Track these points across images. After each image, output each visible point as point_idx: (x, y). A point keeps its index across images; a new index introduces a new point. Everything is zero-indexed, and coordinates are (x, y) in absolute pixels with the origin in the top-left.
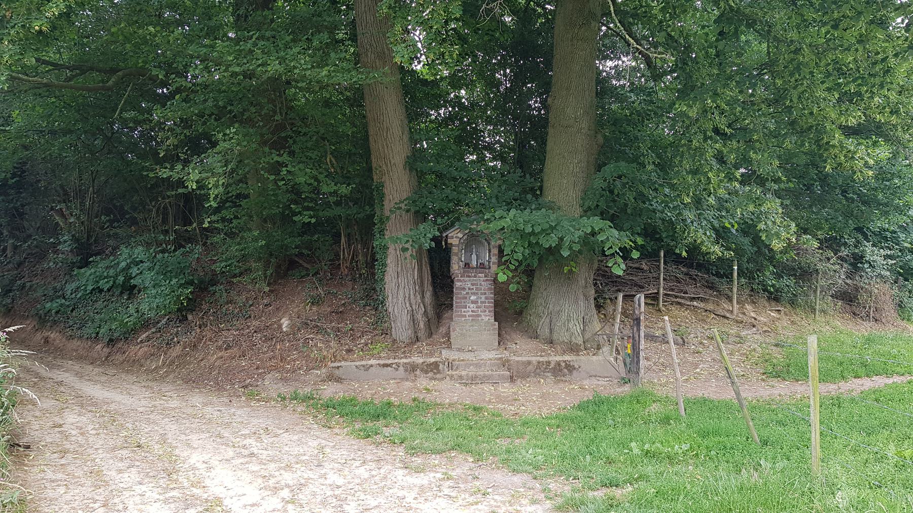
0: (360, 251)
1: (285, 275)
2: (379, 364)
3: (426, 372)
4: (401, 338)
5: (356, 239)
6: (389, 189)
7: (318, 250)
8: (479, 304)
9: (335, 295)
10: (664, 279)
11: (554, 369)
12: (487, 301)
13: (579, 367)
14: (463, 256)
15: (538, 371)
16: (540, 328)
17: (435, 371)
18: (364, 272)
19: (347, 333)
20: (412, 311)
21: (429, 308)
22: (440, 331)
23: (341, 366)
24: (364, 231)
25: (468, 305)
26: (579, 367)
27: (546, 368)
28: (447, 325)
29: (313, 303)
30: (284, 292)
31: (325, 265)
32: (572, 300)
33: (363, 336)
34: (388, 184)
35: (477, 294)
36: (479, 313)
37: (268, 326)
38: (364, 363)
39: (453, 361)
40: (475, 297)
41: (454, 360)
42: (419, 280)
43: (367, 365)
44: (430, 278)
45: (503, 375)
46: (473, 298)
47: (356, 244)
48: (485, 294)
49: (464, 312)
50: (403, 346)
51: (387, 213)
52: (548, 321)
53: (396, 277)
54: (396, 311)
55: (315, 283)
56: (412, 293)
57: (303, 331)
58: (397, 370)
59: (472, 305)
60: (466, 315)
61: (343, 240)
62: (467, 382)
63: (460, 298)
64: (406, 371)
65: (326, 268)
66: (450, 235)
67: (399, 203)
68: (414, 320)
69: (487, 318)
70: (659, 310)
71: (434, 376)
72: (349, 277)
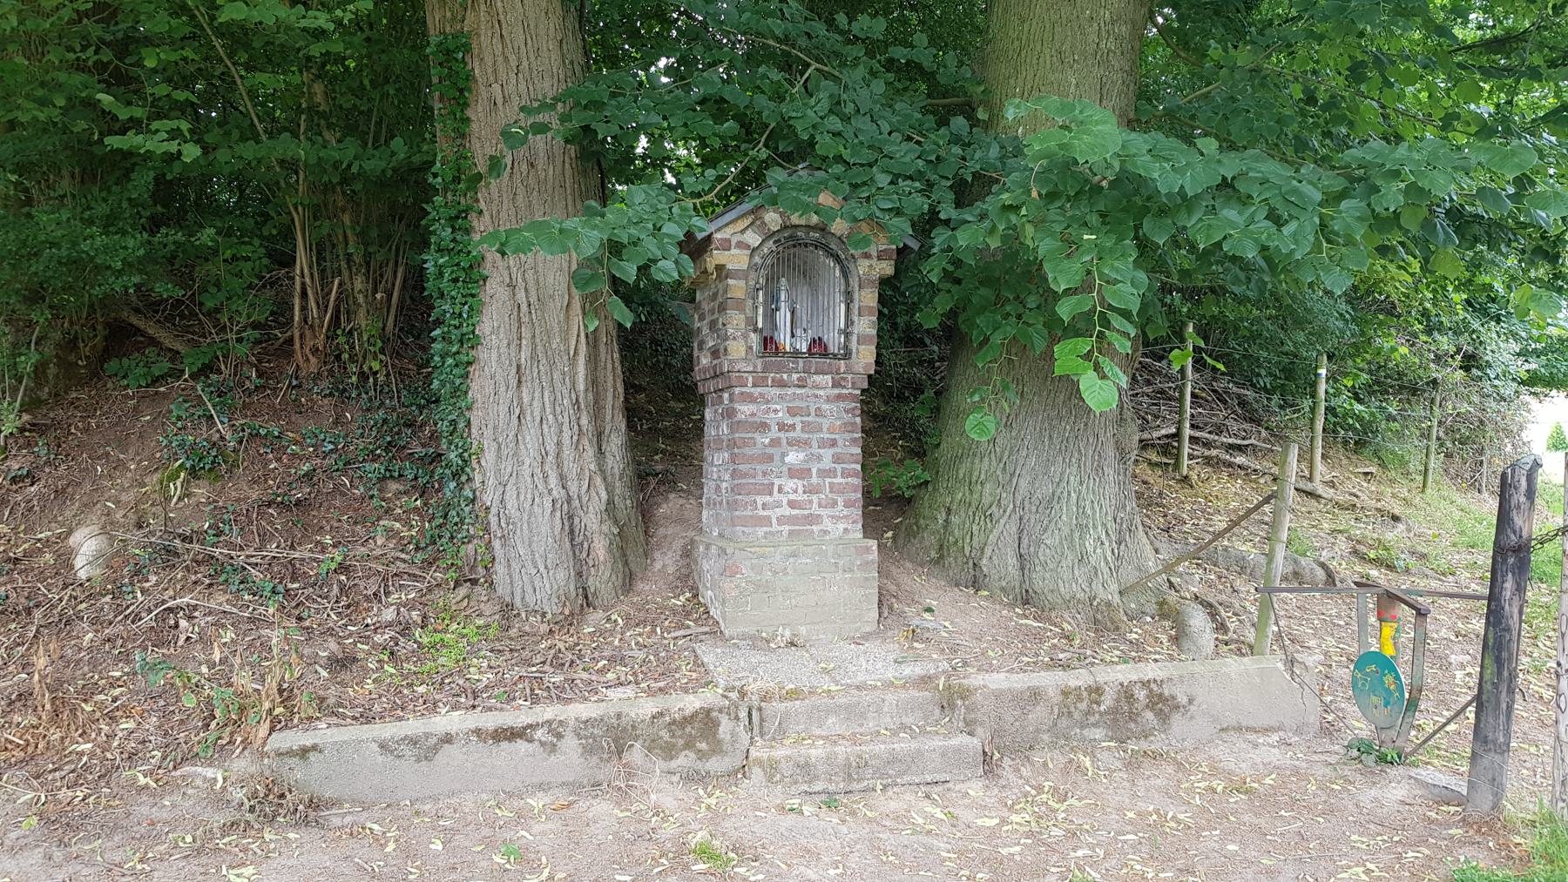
0: (361, 299)
1: (96, 373)
2: (478, 732)
3: (669, 752)
4: (530, 599)
5: (349, 257)
6: (489, 60)
7: (213, 290)
8: (814, 480)
9: (276, 444)
10: (1193, 395)
11: (1114, 711)
12: (839, 467)
13: (1191, 701)
14: (761, 311)
16: (988, 552)
17: (703, 746)
18: (376, 366)
19: (326, 582)
20: (569, 500)
21: (619, 488)
22: (658, 566)
23: (314, 748)
24: (374, 233)
25: (777, 482)
26: (1191, 701)
27: (1088, 713)
28: (678, 545)
29: (193, 473)
30: (86, 430)
31: (240, 340)
32: (1089, 463)
33: (387, 594)
34: (485, 40)
35: (807, 443)
37: (17, 560)
38: (413, 726)
40: (801, 456)
41: (766, 697)
42: (590, 395)
43: (427, 735)
44: (621, 390)
45: (957, 750)
46: (794, 457)
47: (346, 273)
48: (834, 443)
49: (764, 506)
50: (544, 628)
52: (1014, 529)
53: (514, 382)
55: (201, 403)
56: (566, 441)
57: (153, 579)
58: (552, 749)
59: (790, 484)
60: (768, 518)
62: (832, 788)
63: (751, 459)
64: (588, 751)
65: (242, 349)
66: (718, 236)
67: (538, 111)
68: (572, 532)
69: (841, 526)
70: (1185, 479)
72: (325, 384)
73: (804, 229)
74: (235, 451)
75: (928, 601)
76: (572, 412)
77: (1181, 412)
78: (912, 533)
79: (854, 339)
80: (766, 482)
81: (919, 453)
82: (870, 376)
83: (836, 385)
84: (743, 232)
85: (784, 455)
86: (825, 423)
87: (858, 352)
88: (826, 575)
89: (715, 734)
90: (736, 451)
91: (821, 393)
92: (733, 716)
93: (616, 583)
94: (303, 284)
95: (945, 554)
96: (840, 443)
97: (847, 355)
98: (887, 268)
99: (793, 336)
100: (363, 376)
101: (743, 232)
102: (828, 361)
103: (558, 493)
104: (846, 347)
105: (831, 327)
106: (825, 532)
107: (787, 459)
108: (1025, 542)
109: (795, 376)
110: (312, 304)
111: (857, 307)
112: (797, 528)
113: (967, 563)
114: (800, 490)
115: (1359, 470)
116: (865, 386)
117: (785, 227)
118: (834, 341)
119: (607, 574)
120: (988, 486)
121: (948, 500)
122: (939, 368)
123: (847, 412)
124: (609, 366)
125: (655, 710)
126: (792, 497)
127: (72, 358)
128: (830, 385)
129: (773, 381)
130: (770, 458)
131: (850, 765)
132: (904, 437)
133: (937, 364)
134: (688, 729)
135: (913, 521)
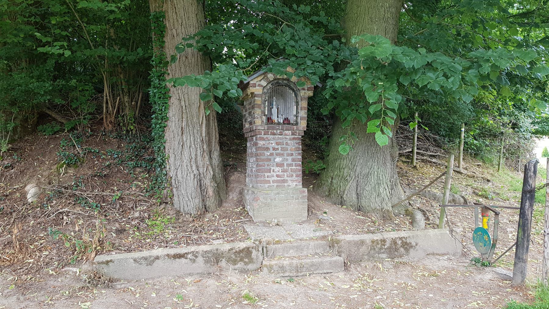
0: (127, 104)
1: (34, 130)
2: (168, 255)
3: (235, 262)
4: (186, 209)
6: (171, 21)
7: (75, 101)
8: (285, 167)
9: (97, 155)
10: (418, 138)
11: (390, 248)
12: (294, 163)
13: (416, 245)
15: (372, 252)
16: (346, 192)
17: (247, 260)
18: (132, 128)
19: (115, 203)
20: (200, 174)
22: (231, 197)
23: (111, 261)
25: (272, 168)
26: (416, 245)
27: (381, 249)
28: (238, 190)
29: (69, 165)
30: (31, 150)
31: (85, 119)
32: (381, 162)
33: (136, 207)
34: (170, 14)
35: (283, 155)
36: (286, 178)
38: (145, 253)
39: (268, 244)
40: (281, 159)
43: (150, 257)
44: (218, 136)
46: (278, 160)
48: (292, 155)
49: (268, 177)
50: (191, 219)
51: (169, 51)
52: (355, 185)
53: (180, 133)
54: (179, 175)
55: (71, 140)
57: (55, 202)
58: (194, 261)
59: (277, 169)
60: (269, 181)
61: (106, 90)
62: (291, 275)
63: (263, 160)
64: (206, 262)
65: (85, 122)
66: (252, 82)
67: (188, 39)
68: (201, 185)
69: (295, 184)
71: (245, 267)
72: (114, 134)
73: (281, 80)
74: (83, 157)
75: (325, 210)
76: (200, 144)
77: (413, 143)
78: (319, 186)
79: (299, 118)
80: (268, 168)
81: (322, 158)
82: (305, 131)
83: (293, 134)
84: (260, 81)
85: (275, 159)
86: (289, 148)
87: (300, 123)
88: (289, 201)
89: (251, 256)
90: (258, 157)
91: (288, 137)
92: (257, 250)
93: (216, 204)
94: (107, 99)
95: (331, 193)
96: (294, 155)
97: (297, 124)
98: (311, 94)
99: (278, 117)
100: (128, 131)
101: (260, 81)
102: (290, 126)
103: (196, 172)
104: (296, 121)
105: (291, 114)
106: (289, 186)
107: (276, 160)
108: (359, 189)
109: (278, 131)
110: (110, 106)
111: (300, 107)
112: (279, 184)
113: (339, 196)
114: (280, 171)
115: (476, 164)
116: (303, 135)
117: (275, 79)
118: (292, 119)
119: (213, 200)
120: (346, 169)
121: (332, 174)
122: (329, 128)
123: (297, 144)
124: (214, 128)
125: (230, 248)
126: (278, 173)
127: (26, 125)
128: (291, 134)
129: (271, 133)
130: (270, 160)
131: (298, 267)
132: (317, 152)
133: (328, 127)
134: (241, 254)
135: (320, 182)
